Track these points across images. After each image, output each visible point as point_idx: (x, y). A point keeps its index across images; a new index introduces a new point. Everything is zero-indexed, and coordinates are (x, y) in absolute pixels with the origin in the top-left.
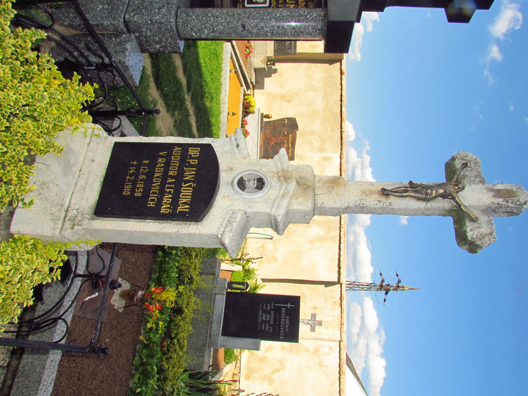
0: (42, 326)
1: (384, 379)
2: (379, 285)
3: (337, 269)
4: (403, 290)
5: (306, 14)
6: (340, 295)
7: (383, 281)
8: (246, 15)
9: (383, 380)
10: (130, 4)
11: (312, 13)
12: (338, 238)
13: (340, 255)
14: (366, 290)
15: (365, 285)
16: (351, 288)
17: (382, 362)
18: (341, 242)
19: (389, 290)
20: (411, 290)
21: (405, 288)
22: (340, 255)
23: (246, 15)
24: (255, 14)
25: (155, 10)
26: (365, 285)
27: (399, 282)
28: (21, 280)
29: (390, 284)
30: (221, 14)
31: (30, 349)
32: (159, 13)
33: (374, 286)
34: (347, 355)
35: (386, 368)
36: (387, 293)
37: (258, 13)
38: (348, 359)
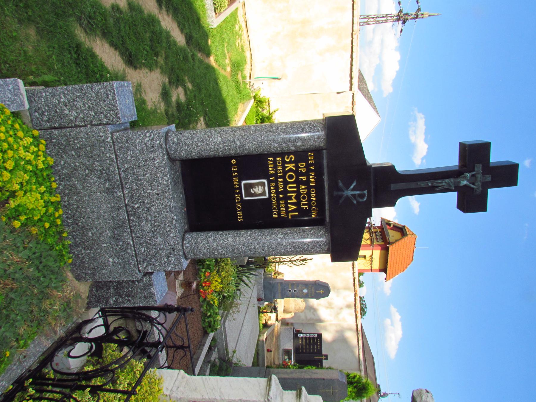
0: (129, 310)
1: (397, 72)
2: (396, 15)
3: (349, 79)
4: (422, 18)
5: (310, 249)
6: (352, 100)
7: (401, 11)
8: (252, 253)
9: (395, 74)
10: (137, 252)
11: (316, 248)
12: (351, 46)
13: (352, 65)
14: (382, 23)
15: (381, 17)
16: (364, 23)
17: (397, 56)
18: (353, 51)
19: (407, 20)
20: (431, 17)
21: (424, 16)
22: (352, 65)
23: (252, 253)
24: (260, 251)
25: (164, 259)
26: (381, 17)
27: (419, 10)
28: (76, 211)
29: (408, 12)
30: (227, 253)
31: (62, 96)
32: (169, 262)
33: (391, 17)
34: (359, 71)
35: (401, 62)
36: (404, 23)
37: (263, 250)
38: (361, 79)
